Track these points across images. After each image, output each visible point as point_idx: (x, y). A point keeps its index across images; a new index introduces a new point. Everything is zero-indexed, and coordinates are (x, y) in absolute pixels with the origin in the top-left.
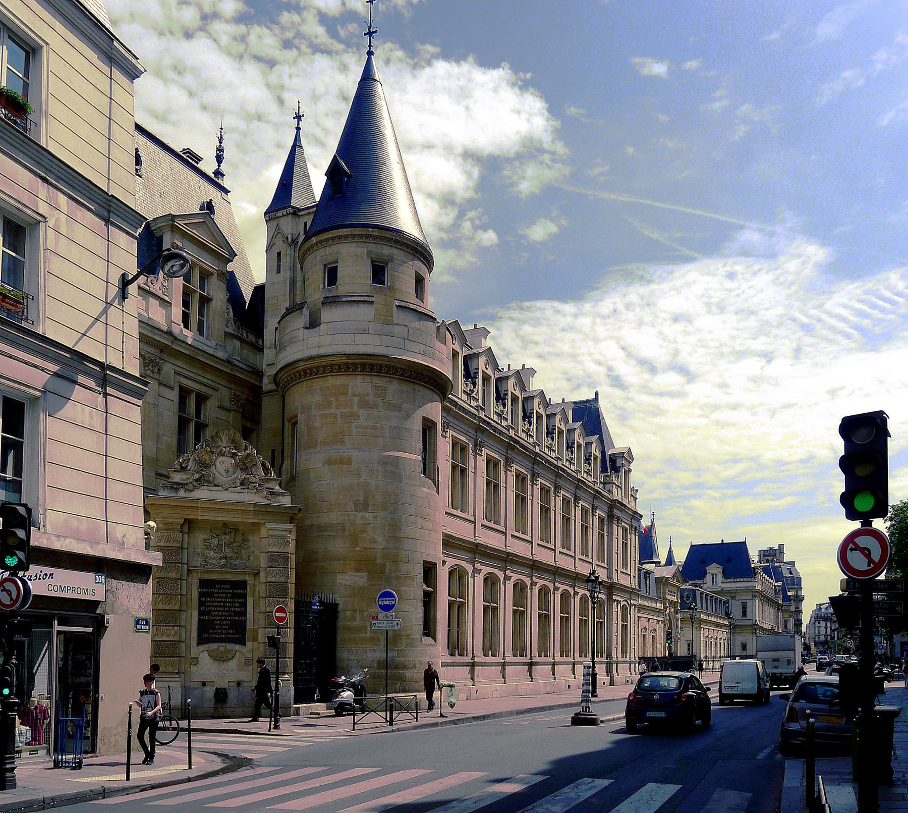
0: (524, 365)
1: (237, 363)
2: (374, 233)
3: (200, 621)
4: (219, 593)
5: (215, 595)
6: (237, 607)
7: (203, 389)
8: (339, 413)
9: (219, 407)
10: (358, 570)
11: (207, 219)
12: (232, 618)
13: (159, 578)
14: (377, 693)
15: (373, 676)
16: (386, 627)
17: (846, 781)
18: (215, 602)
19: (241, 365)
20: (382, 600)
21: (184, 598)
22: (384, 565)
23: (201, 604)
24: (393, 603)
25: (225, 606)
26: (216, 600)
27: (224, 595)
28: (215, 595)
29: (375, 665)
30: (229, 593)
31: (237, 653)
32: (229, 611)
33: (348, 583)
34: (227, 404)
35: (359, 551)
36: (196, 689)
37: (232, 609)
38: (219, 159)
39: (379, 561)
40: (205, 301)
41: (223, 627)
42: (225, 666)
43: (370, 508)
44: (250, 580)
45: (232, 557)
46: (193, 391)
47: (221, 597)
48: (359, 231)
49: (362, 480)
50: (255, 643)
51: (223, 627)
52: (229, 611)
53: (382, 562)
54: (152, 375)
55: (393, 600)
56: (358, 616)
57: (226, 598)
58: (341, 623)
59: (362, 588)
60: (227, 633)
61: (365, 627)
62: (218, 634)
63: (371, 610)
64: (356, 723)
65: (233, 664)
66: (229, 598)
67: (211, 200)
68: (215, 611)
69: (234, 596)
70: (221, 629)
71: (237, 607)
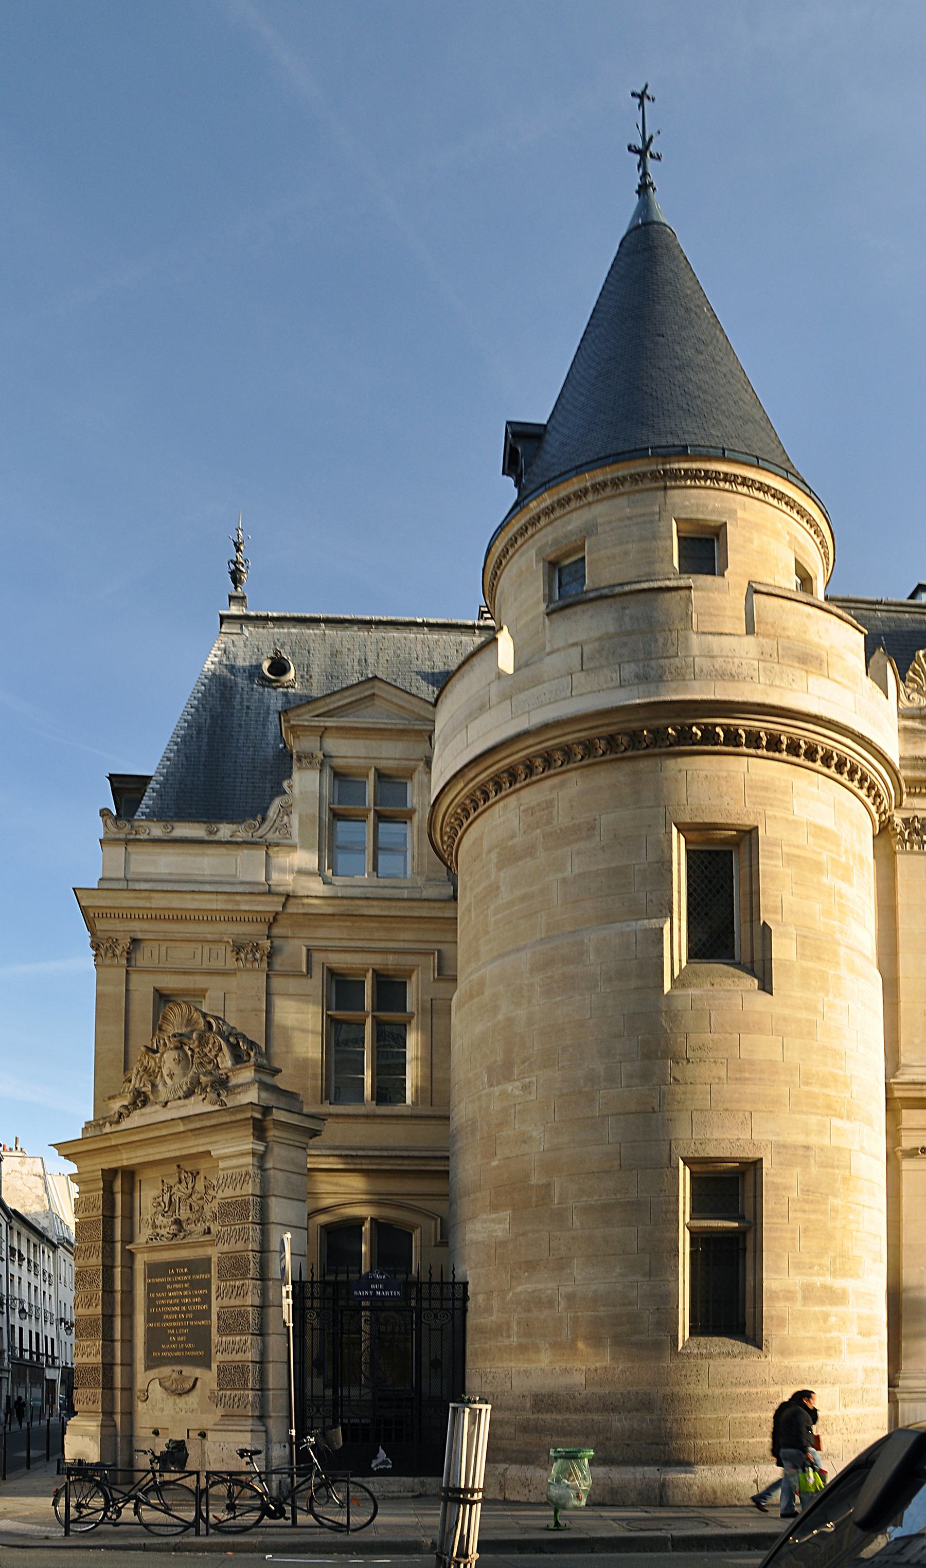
0: (633, 95)
2: (543, 505)
4: (172, 1283)
5: (169, 1287)
6: (196, 1303)
12: (191, 1323)
14: (532, 1463)
15: (524, 1428)
17: (314, 1003)
18: (168, 1297)
22: (548, 1186)
25: (181, 1304)
26: (170, 1294)
28: (169, 1287)
29: (528, 1405)
30: (186, 1281)
32: (188, 1311)
33: (480, 1239)
35: (497, 1166)
36: (146, 1439)
41: (179, 1339)
42: (182, 1402)
43: (516, 1071)
45: (188, 1219)
48: (517, 523)
51: (179, 1339)
52: (188, 1311)
53: (544, 1181)
56: (495, 1303)
57: (182, 1290)
58: (472, 1320)
59: (503, 1244)
60: (185, 1349)
61: (508, 1324)
62: (174, 1350)
63: (519, 1289)
65: (192, 1400)
66: (186, 1289)
68: (168, 1313)
69: (195, 1285)
70: (177, 1342)
71: (196, 1303)
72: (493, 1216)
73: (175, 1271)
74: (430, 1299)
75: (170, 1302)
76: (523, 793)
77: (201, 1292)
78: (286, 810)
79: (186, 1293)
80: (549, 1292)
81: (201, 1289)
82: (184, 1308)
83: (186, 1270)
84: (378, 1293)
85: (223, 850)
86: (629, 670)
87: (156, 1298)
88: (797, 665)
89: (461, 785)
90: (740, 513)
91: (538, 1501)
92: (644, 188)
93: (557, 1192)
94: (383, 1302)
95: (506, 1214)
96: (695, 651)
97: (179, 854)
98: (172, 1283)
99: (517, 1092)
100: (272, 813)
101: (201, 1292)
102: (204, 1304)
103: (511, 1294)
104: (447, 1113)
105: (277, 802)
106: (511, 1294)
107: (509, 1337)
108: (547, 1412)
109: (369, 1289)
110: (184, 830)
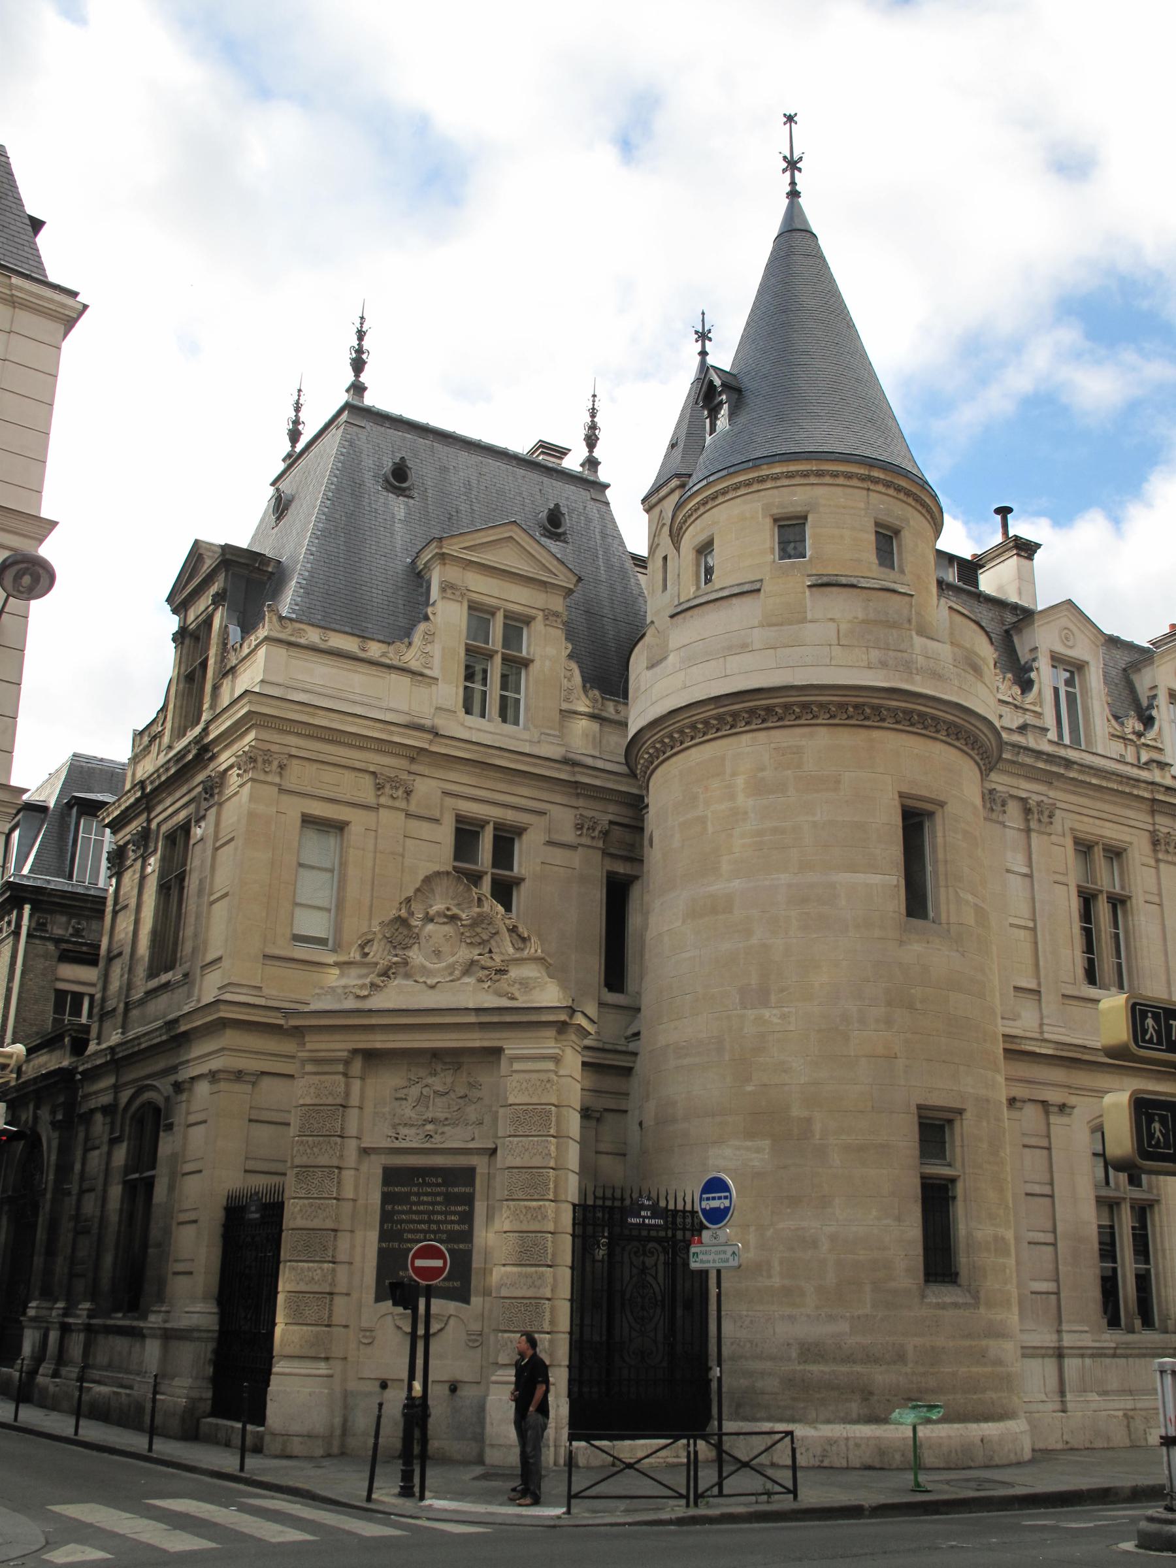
1: (589, 761)
3: (381, 1252)
4: (418, 1194)
5: (414, 1199)
6: (452, 1222)
7: (510, 816)
8: (709, 815)
9: (550, 843)
10: (750, 1135)
11: (515, 533)
13: (301, 1167)
16: (714, 1261)
18: (411, 1212)
19: (600, 764)
20: (708, 1199)
21: (347, 1207)
22: (809, 1120)
23: (386, 1217)
24: (727, 1203)
25: (430, 1222)
27: (429, 1199)
28: (414, 1199)
30: (439, 1194)
31: (452, 1322)
34: (570, 836)
37: (443, 1227)
38: (591, 441)
39: (796, 1112)
40: (516, 665)
44: (480, 1164)
46: (488, 822)
47: (424, 1203)
49: (754, 941)
50: (487, 1298)
54: (390, 803)
55: (726, 1198)
57: (433, 1204)
63: (781, 1226)
64: (576, 1496)
66: (439, 1203)
67: (557, 505)
69: (450, 1199)
71: (452, 1222)
72: (749, 1144)
73: (424, 1180)
74: (684, 1229)
75: (414, 1217)
76: (773, 732)
77: (459, 1209)
78: (429, 637)
79: (438, 1208)
80: (813, 1231)
81: (461, 1205)
82: (434, 1227)
83: (440, 1180)
84: (647, 1221)
85: (373, 670)
86: (875, 654)
87: (394, 1212)
88: (972, 672)
89: (713, 707)
90: (912, 523)
91: (811, 1465)
92: (794, 194)
93: (817, 1127)
94: (649, 1231)
95: (766, 1143)
96: (917, 650)
97: (333, 666)
98: (418, 1194)
99: (775, 1020)
100: (417, 638)
101: (459, 1209)
102: (464, 1223)
103: (772, 1230)
104: (601, 1010)
105: (422, 627)
106: (772, 1230)
107: (770, 1276)
108: (814, 1362)
109: (639, 1216)
110: (339, 641)
